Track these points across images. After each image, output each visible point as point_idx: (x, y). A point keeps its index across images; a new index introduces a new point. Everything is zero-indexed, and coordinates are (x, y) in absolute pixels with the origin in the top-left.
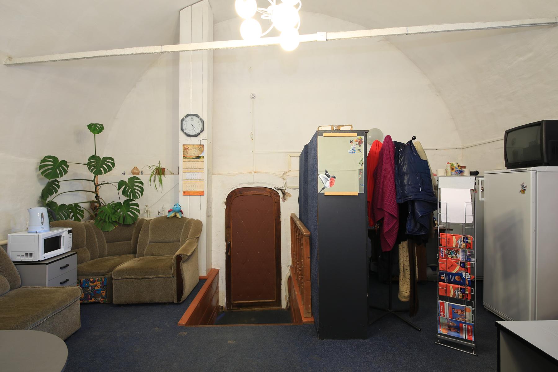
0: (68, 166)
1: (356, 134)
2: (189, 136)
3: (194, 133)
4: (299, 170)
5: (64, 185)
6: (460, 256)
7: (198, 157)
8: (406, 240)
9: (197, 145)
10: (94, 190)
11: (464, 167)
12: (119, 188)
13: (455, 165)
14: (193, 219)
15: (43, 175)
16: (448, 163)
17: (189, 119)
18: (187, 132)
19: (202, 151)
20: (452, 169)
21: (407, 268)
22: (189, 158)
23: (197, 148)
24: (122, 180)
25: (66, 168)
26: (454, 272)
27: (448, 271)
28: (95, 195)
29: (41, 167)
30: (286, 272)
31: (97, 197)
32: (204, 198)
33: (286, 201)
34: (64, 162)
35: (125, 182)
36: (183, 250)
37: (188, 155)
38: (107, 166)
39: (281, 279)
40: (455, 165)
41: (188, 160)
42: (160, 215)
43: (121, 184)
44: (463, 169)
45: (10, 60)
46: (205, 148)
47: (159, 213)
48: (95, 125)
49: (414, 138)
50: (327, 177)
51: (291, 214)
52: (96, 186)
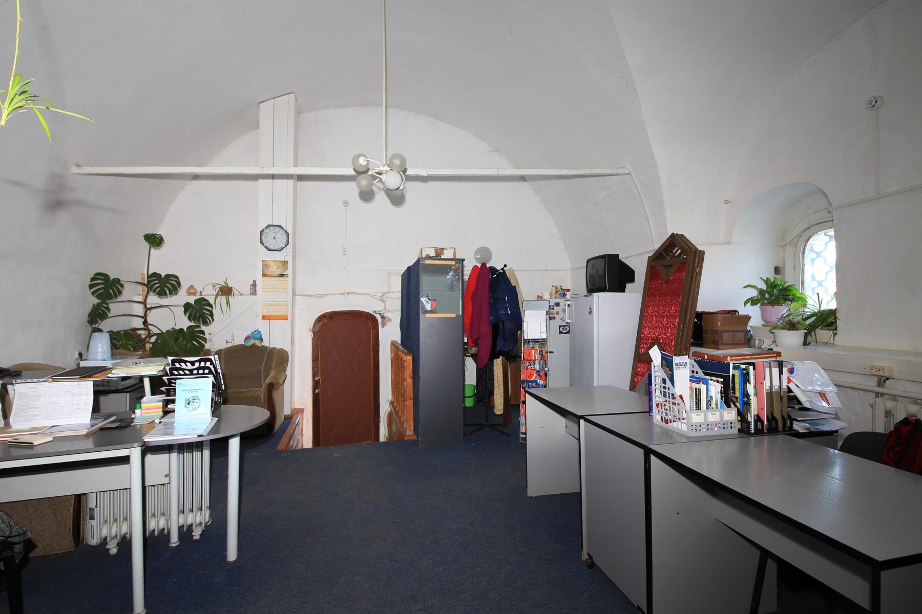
0: (122, 286)
1: (454, 262)
2: (269, 250)
3: (277, 248)
4: (401, 291)
5: (115, 308)
6: (537, 367)
7: (282, 275)
8: (499, 358)
9: (280, 261)
10: (143, 315)
11: (569, 290)
12: (185, 312)
13: (559, 288)
14: (274, 348)
15: (95, 296)
16: (553, 286)
17: (270, 230)
18: (268, 246)
19: (286, 269)
20: (557, 292)
21: (501, 383)
22: (270, 276)
23: (280, 265)
24: (188, 303)
25: (120, 288)
26: (532, 379)
27: (528, 379)
28: (143, 320)
29: (91, 287)
30: (385, 408)
31: (145, 322)
32: (288, 323)
33: (385, 327)
34: (117, 281)
35: (192, 304)
36: (273, 378)
37: (268, 273)
38: (172, 285)
39: (379, 417)
40: (559, 288)
41: (269, 278)
42: (229, 345)
43: (187, 307)
44: (567, 293)
45: (79, 168)
46: (290, 265)
47: (227, 342)
48: (154, 235)
49: (505, 266)
50: (428, 300)
51: (392, 341)
52: (147, 309)
